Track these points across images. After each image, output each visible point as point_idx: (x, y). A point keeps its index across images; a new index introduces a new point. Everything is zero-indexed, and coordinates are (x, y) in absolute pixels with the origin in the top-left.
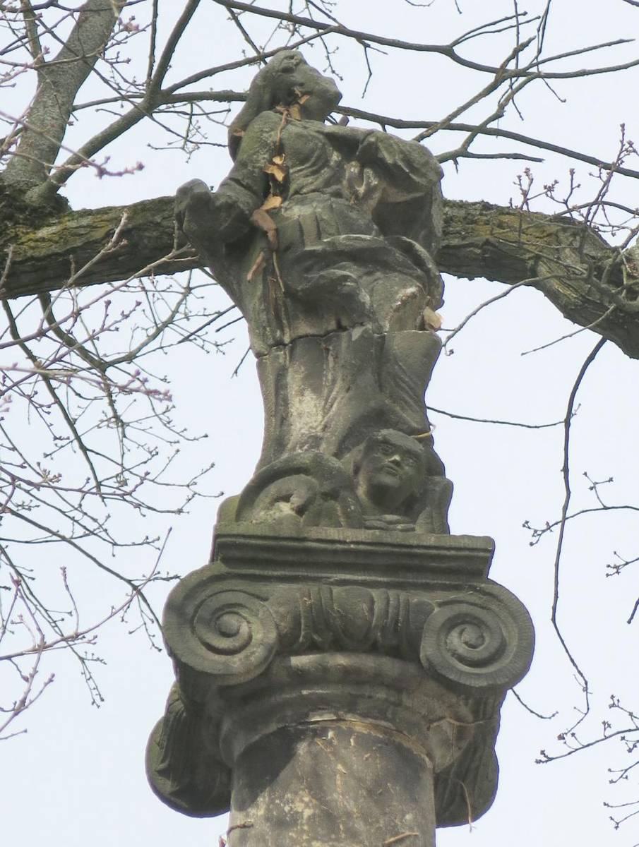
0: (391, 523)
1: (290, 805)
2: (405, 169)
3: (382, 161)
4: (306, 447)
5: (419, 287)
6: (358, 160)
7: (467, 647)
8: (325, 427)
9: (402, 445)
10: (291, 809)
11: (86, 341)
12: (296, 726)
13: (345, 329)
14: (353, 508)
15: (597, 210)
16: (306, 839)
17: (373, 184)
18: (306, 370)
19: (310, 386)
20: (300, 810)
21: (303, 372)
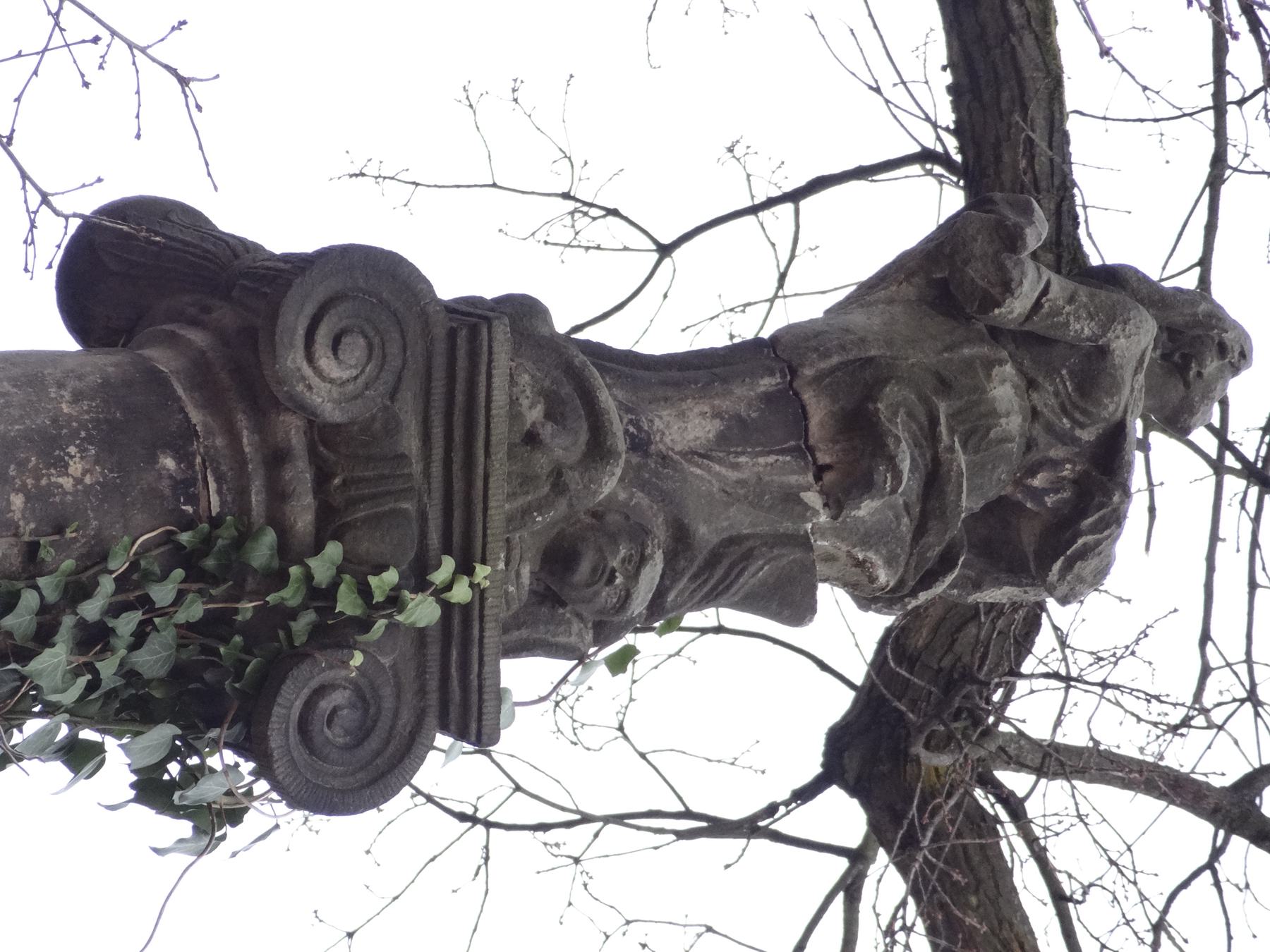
0: (518, 575)
1: (78, 455)
2: (1071, 550)
3: (1084, 514)
4: (631, 429)
5: (887, 586)
6: (1085, 475)
7: (328, 712)
8: (664, 459)
9: (639, 586)
10: (72, 457)
12: (200, 454)
13: (818, 478)
14: (539, 519)
16: (27, 485)
17: (1046, 499)
18: (753, 419)
19: (728, 428)
20: (71, 470)
21: (749, 416)
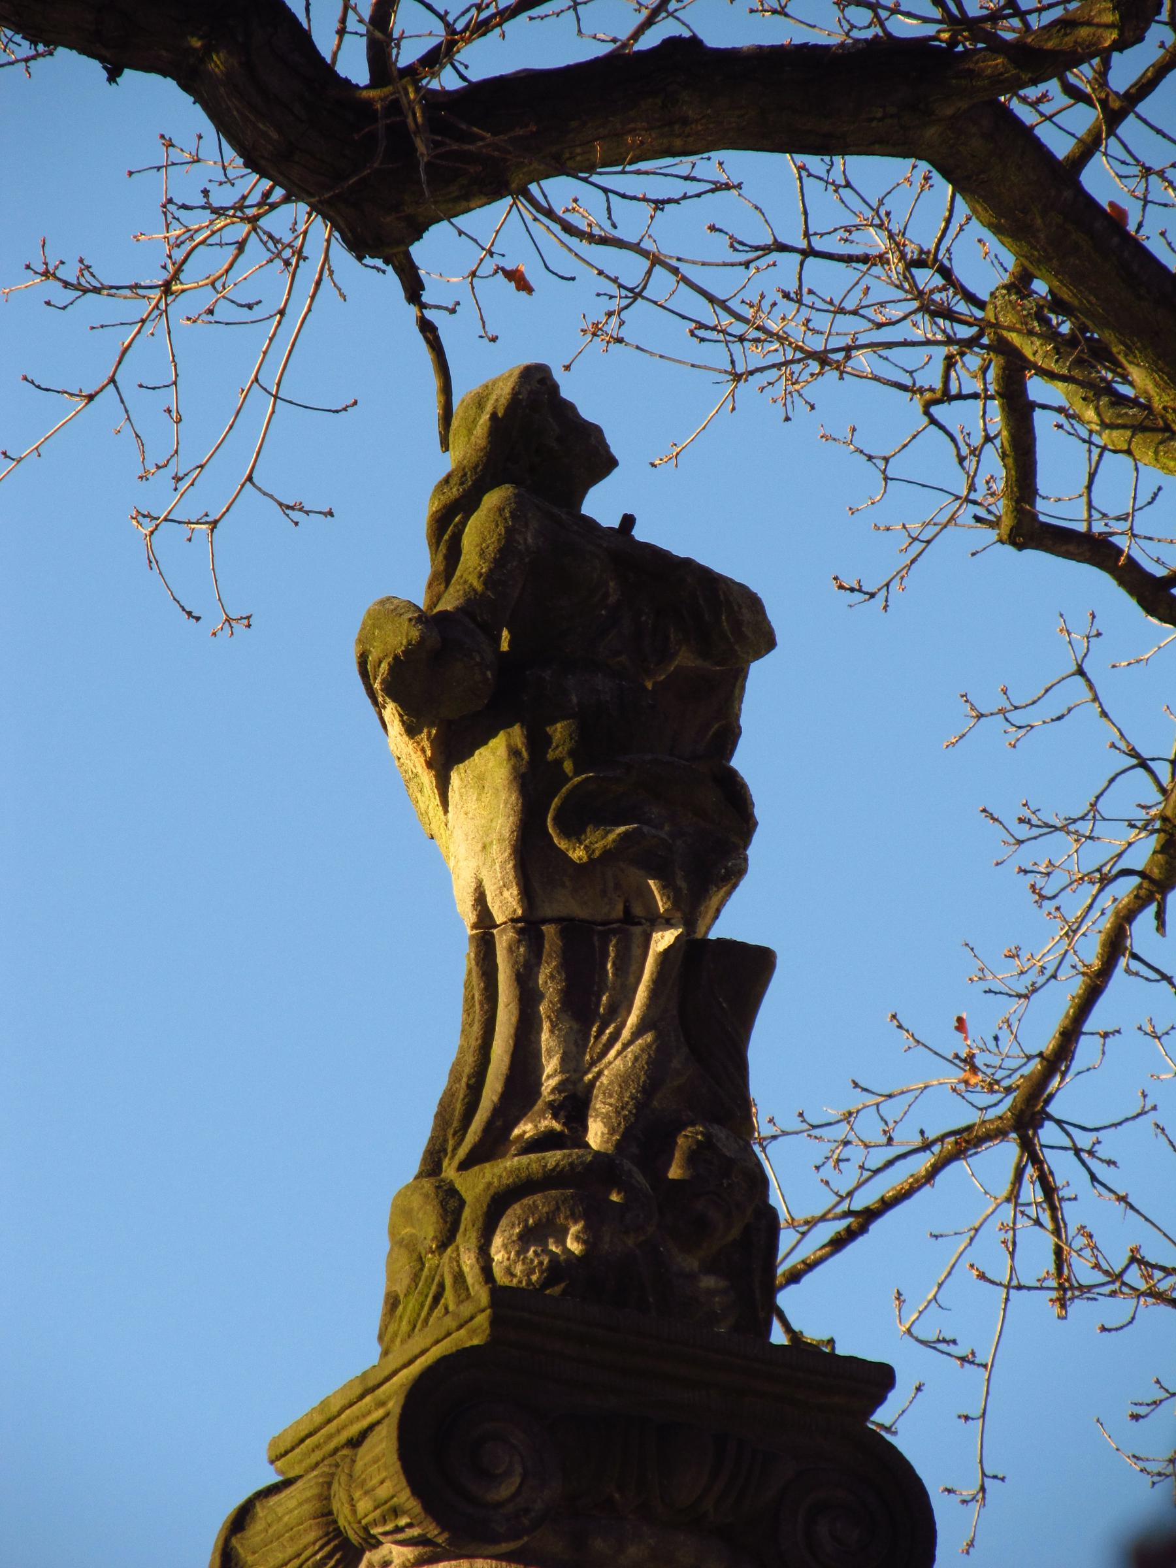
11: (933, 1153)
15: (842, 27)
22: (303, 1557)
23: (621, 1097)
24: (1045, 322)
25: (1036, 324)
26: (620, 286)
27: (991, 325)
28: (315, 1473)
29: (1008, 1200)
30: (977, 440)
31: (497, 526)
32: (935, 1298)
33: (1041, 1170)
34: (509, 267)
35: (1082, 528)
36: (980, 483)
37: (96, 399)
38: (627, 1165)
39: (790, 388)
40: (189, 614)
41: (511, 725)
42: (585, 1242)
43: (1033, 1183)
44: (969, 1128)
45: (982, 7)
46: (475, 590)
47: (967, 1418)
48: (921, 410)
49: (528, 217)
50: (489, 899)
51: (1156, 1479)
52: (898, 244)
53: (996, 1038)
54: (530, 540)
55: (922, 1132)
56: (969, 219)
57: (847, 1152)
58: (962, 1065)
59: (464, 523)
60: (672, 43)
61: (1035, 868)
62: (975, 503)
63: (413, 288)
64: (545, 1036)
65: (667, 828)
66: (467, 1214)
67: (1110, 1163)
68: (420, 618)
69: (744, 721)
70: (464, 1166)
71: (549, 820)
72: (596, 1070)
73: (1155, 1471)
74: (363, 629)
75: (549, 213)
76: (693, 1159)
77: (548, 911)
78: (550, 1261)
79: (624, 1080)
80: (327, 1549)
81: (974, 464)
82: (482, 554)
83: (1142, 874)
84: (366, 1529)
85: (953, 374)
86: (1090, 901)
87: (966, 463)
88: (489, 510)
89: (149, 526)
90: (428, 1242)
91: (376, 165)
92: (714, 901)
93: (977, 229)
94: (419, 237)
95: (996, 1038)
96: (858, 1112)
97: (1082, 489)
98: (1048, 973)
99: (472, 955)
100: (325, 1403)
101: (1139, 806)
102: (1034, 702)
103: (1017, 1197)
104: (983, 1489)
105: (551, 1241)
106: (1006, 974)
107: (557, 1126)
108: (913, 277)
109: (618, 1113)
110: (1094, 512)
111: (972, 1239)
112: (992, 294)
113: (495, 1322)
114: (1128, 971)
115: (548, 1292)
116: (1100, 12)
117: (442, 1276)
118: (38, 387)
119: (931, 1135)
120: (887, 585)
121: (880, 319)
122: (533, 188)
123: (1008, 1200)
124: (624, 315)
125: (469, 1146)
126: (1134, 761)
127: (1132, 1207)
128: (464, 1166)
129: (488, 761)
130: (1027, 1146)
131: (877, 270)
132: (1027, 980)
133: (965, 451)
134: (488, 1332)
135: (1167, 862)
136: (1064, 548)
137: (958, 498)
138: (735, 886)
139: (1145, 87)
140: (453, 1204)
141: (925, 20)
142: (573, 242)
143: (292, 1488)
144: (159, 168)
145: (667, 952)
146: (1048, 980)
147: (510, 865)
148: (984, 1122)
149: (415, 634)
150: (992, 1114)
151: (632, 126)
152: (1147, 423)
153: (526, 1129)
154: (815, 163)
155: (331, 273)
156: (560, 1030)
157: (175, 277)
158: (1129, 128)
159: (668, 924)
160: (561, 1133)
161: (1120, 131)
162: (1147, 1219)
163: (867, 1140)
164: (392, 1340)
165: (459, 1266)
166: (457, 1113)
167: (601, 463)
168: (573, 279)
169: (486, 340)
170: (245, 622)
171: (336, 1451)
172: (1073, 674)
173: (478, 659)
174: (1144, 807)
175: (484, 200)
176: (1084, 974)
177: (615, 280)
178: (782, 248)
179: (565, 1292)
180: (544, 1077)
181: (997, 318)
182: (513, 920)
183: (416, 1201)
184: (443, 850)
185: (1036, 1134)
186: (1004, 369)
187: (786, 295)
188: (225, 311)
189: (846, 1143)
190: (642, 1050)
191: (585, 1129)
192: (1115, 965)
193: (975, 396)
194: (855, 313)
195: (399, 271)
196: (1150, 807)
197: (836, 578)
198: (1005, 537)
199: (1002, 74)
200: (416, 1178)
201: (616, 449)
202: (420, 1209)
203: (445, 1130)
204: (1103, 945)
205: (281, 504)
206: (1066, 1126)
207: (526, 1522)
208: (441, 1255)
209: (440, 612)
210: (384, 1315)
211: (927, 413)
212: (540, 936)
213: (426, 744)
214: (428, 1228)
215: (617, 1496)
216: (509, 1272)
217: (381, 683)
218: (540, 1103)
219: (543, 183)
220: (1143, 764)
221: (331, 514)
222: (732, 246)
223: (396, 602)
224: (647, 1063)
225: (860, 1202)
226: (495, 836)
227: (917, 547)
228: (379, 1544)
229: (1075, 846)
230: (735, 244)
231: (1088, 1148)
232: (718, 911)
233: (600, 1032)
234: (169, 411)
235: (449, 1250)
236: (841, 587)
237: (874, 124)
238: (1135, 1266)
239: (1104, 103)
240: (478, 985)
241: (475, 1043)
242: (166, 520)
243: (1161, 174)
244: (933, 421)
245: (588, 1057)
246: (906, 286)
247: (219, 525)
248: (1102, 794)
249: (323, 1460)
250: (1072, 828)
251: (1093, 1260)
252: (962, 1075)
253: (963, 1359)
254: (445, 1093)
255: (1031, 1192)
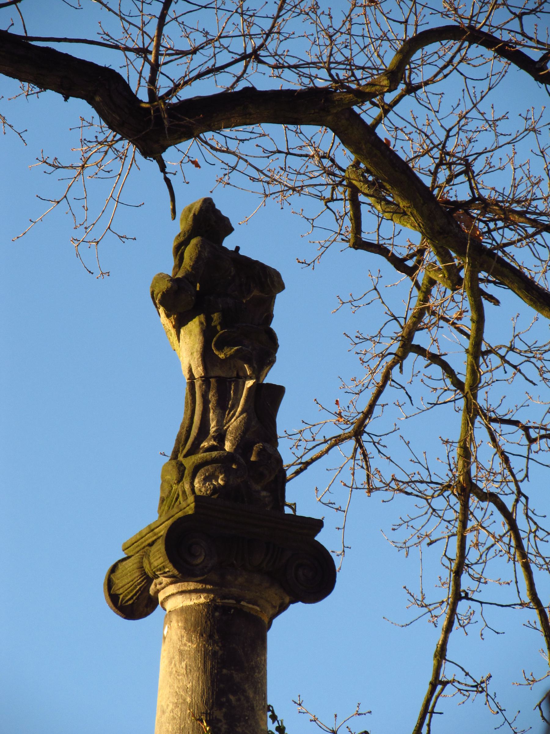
22: (134, 581)
23: (235, 435)
24: (364, 177)
25: (362, 178)
26: (229, 166)
27: (347, 178)
28: (138, 554)
29: (352, 458)
30: (343, 213)
31: (196, 250)
32: (328, 490)
33: (363, 450)
34: (193, 160)
35: (376, 242)
36: (343, 228)
37: (60, 203)
38: (238, 456)
39: (283, 198)
40: (90, 272)
41: (200, 314)
42: (224, 481)
43: (361, 454)
44: (340, 436)
45: (344, 76)
46: (188, 270)
47: (339, 529)
48: (324, 204)
49: (200, 144)
50: (193, 370)
51: (400, 549)
52: (317, 151)
53: (348, 407)
54: (206, 255)
55: (324, 437)
56: (340, 143)
57: (300, 443)
58: (337, 416)
59: (185, 249)
60: (246, 89)
61: (361, 352)
62: (342, 234)
63: (163, 167)
64: (211, 414)
65: (250, 347)
66: (186, 472)
67: (385, 446)
68: (171, 280)
69: (274, 313)
70: (185, 456)
71: (213, 344)
72: (228, 425)
73: (400, 546)
74: (152, 283)
75: (206, 143)
76: (259, 454)
77: (212, 374)
78: (213, 487)
79: (237, 429)
80: (142, 579)
81: (341, 222)
82: (191, 259)
83: (395, 354)
84: (154, 572)
85: (334, 192)
86: (378, 363)
87: (339, 221)
88: (193, 245)
89: (77, 243)
90: (174, 481)
91: (151, 128)
92: (266, 371)
93: (342, 146)
94: (165, 151)
95: (348, 407)
96: (304, 430)
97: (376, 230)
98: (365, 386)
99: (188, 388)
100: (140, 532)
101: (395, 333)
102: (360, 299)
103: (355, 458)
104: (344, 551)
105: (213, 480)
106: (351, 386)
107: (215, 443)
108: (322, 162)
109: (235, 439)
110: (380, 237)
111: (340, 471)
112: (347, 168)
113: (196, 507)
114: (391, 385)
115: (212, 497)
116: (383, 80)
117: (179, 492)
118: (42, 199)
119: (327, 438)
120: (314, 261)
121: (311, 176)
122: (201, 135)
123: (352, 458)
124: (230, 175)
125: (187, 450)
126: (393, 318)
127: (392, 461)
128: (185, 456)
129: (193, 326)
130: (358, 441)
131: (311, 160)
132: (358, 389)
133: (338, 217)
134: (194, 510)
135: (403, 351)
136: (370, 249)
137: (336, 233)
138: (272, 366)
139: (396, 102)
140: (182, 468)
141: (326, 80)
142: (214, 152)
143: (130, 559)
144: (80, 128)
145: (250, 388)
146: (365, 389)
147: (200, 359)
148: (344, 434)
149: (169, 285)
150: (347, 431)
151: (234, 115)
152: (398, 211)
153: (205, 444)
154: (291, 127)
155: (135, 161)
156: (216, 412)
157: (86, 163)
158: (391, 115)
159: (251, 378)
160: (216, 446)
161: (388, 116)
162: (396, 465)
163: (307, 440)
164: (162, 512)
165: (184, 488)
166: (183, 439)
167: (228, 229)
168: (214, 165)
169: (185, 183)
170: (108, 274)
171: (144, 547)
172: (373, 290)
173: (190, 293)
174: (396, 333)
175: (186, 139)
176: (377, 386)
177: (227, 164)
178: (280, 152)
179: (218, 497)
180: (211, 428)
181: (349, 176)
182: (201, 377)
183: (170, 467)
184: (178, 354)
185: (361, 437)
186: (351, 192)
187: (282, 169)
188: (102, 174)
189: (300, 440)
190: (243, 419)
191: (224, 444)
192: (387, 383)
193: (342, 199)
194: (304, 174)
195: (158, 162)
196: (398, 333)
197: (297, 259)
198: (351, 246)
199: (352, 99)
200: (170, 460)
201: (234, 225)
202: (171, 470)
203: (179, 445)
204: (383, 377)
205: (119, 236)
206: (371, 435)
207: (206, 570)
208: (178, 485)
209: (177, 278)
210: (160, 504)
211: (326, 205)
212: (210, 382)
213: (173, 320)
214: (173, 476)
215: (235, 562)
216: (200, 491)
217: (159, 301)
218: (210, 436)
219: (205, 134)
220: (396, 319)
221: (135, 239)
222: (263, 151)
223: (163, 274)
224: (244, 423)
225: (304, 460)
226: (195, 350)
227: (324, 249)
228: (159, 577)
229: (374, 345)
230: (265, 151)
231: (377, 442)
232: (267, 374)
233: (229, 413)
234: (84, 207)
235: (181, 483)
236: (299, 262)
237: (311, 115)
238: (393, 481)
239: (383, 107)
240: (189, 398)
241: (188, 416)
242: (82, 241)
243: (402, 130)
244: (328, 208)
245: (225, 421)
246: (320, 165)
247: (99, 243)
248: (382, 328)
249: (140, 550)
250: (373, 339)
251: (380, 479)
252: (337, 419)
253: (337, 509)
254: (179, 433)
255: (359, 456)
